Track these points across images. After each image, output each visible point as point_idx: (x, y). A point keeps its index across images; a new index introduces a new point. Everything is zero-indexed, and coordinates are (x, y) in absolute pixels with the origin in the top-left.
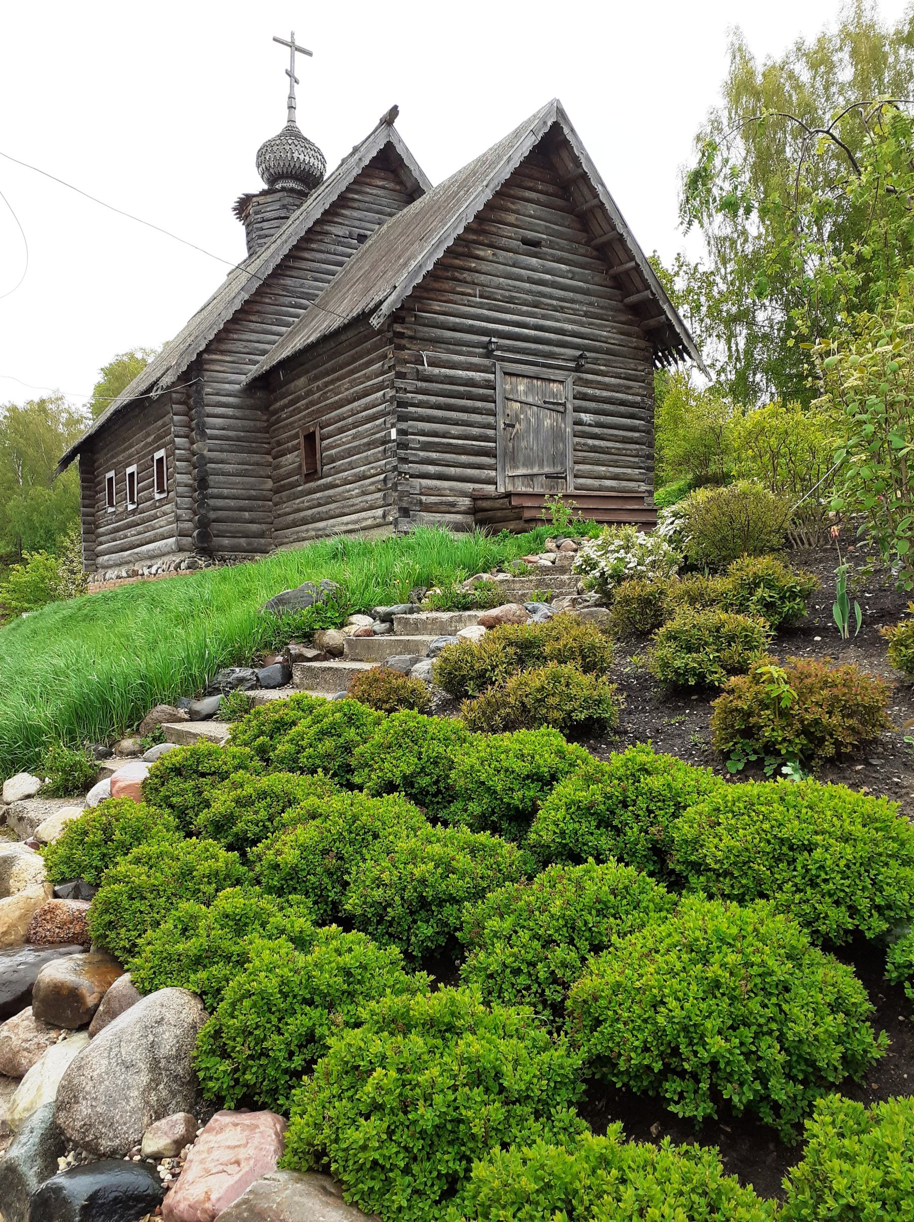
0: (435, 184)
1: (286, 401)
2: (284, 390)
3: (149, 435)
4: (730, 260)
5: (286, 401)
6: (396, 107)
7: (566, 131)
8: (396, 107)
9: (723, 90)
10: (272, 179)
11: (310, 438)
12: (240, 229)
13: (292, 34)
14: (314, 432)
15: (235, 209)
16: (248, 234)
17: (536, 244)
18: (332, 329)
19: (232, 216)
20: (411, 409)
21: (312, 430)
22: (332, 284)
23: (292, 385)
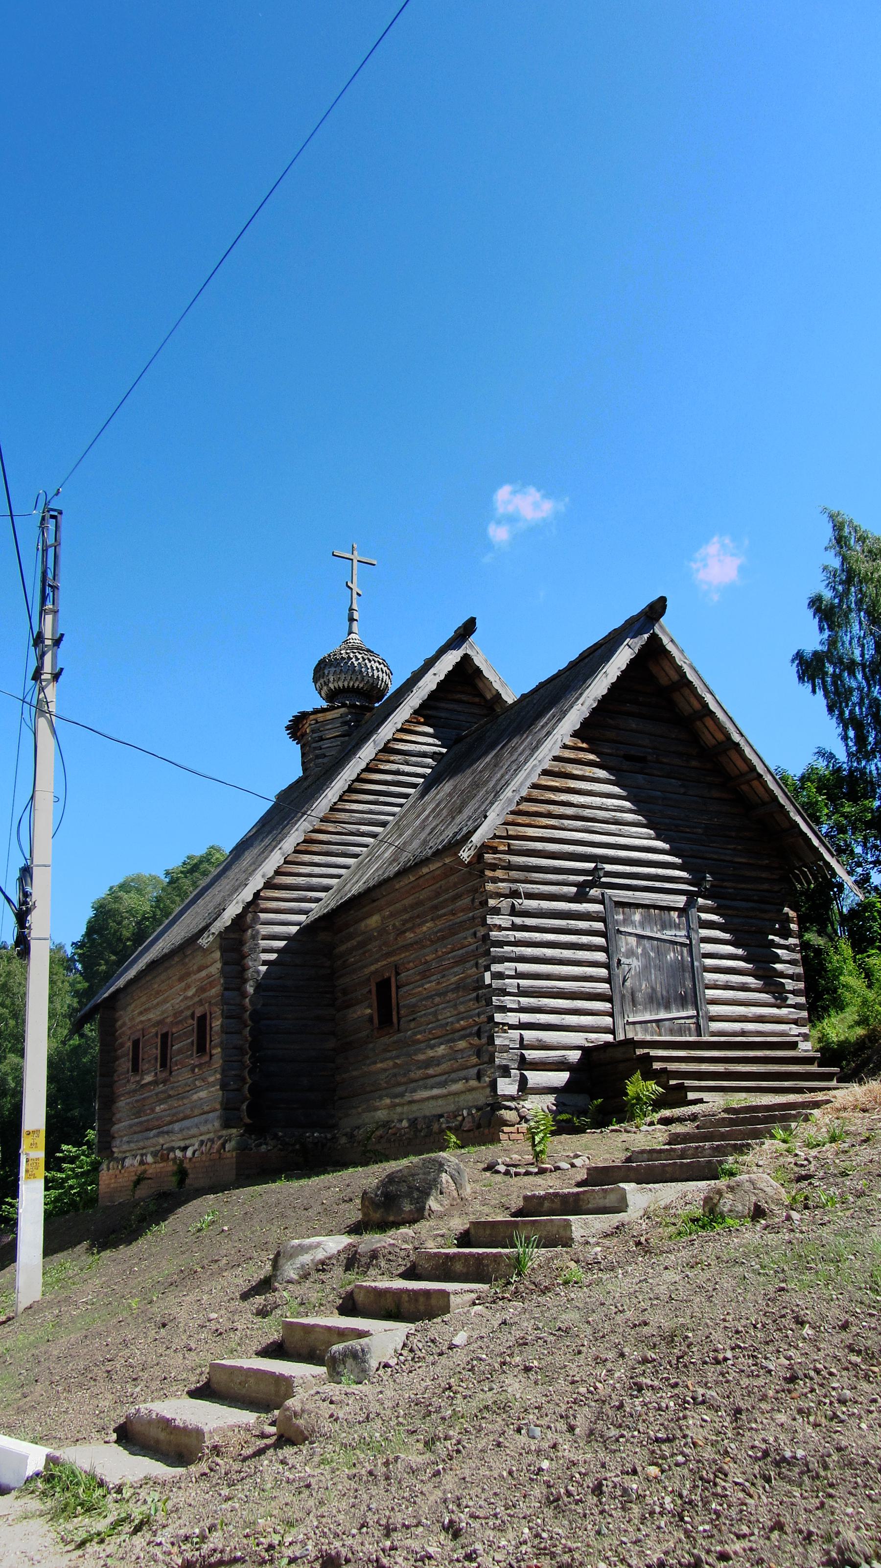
0: (510, 697)
1: (354, 942)
2: (351, 929)
3: (188, 987)
4: (346, 1135)
5: (354, 942)
6: (662, 600)
7: (665, 640)
8: (662, 600)
9: (813, 595)
10: (331, 696)
11: (384, 987)
12: (295, 749)
13: (826, 549)
14: (389, 979)
15: (288, 728)
16: (303, 755)
17: (642, 760)
18: (166, 951)
19: (285, 735)
20: (507, 949)
21: (387, 975)
22: (406, 808)
23: (363, 924)
